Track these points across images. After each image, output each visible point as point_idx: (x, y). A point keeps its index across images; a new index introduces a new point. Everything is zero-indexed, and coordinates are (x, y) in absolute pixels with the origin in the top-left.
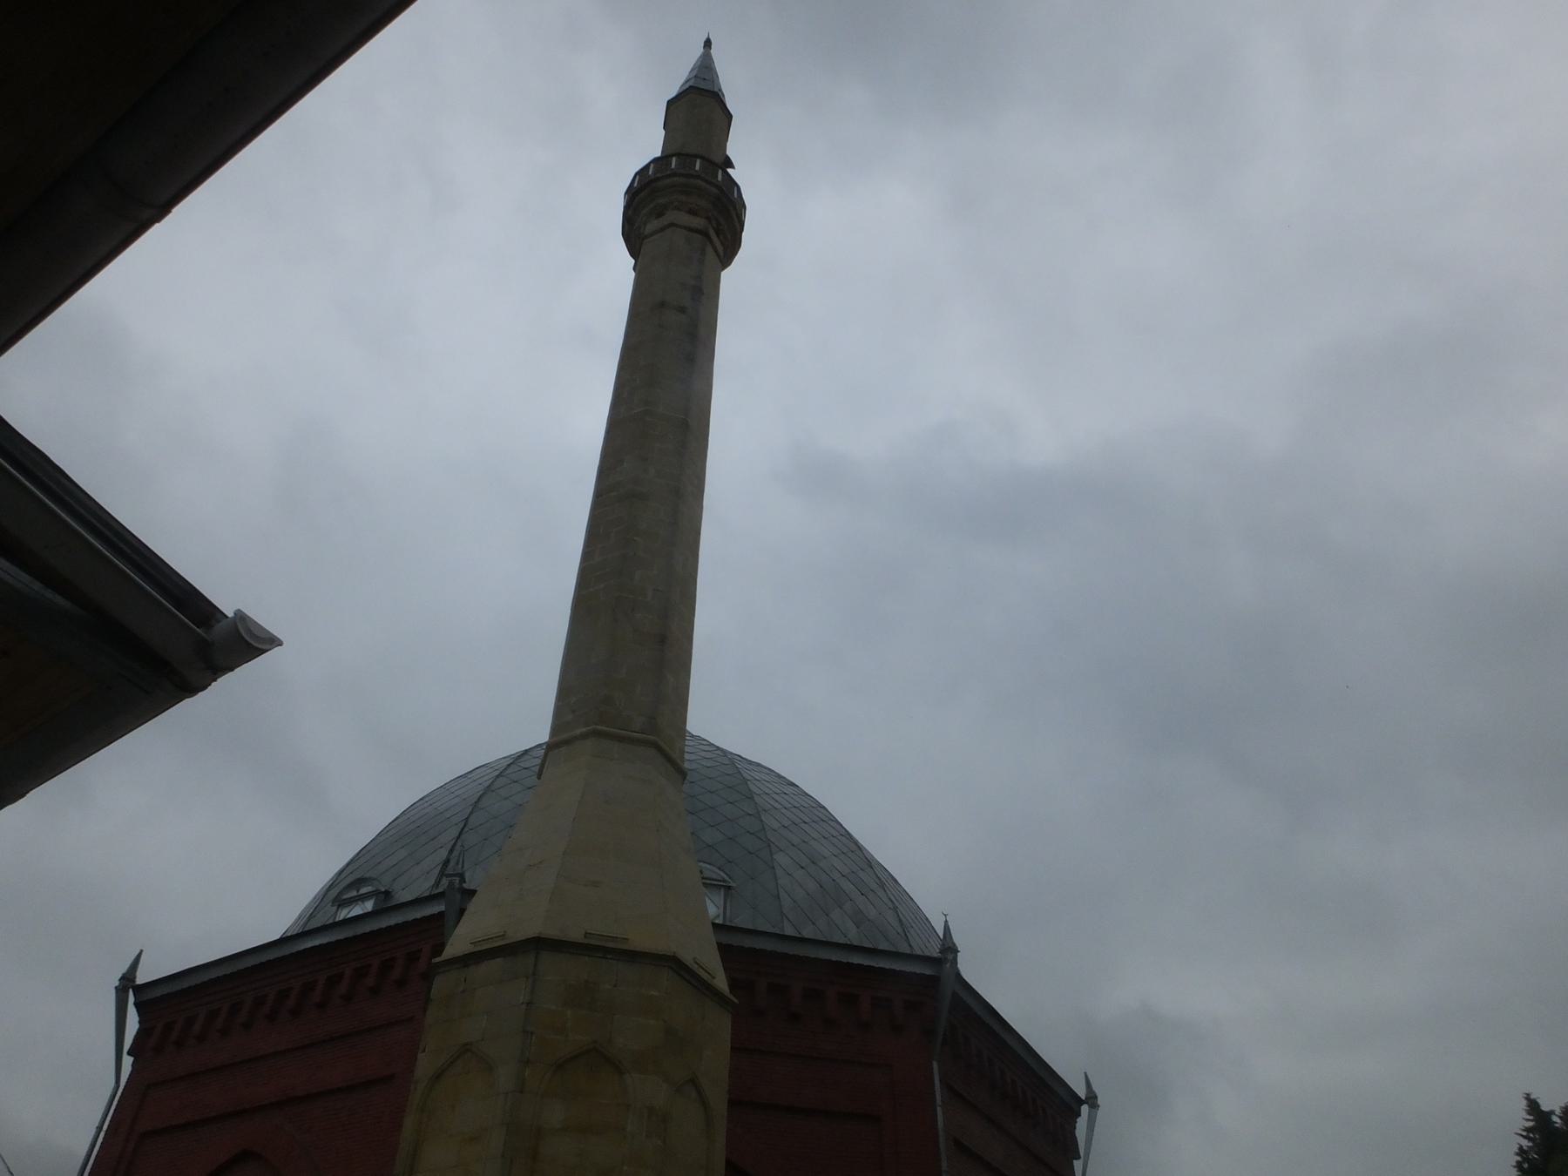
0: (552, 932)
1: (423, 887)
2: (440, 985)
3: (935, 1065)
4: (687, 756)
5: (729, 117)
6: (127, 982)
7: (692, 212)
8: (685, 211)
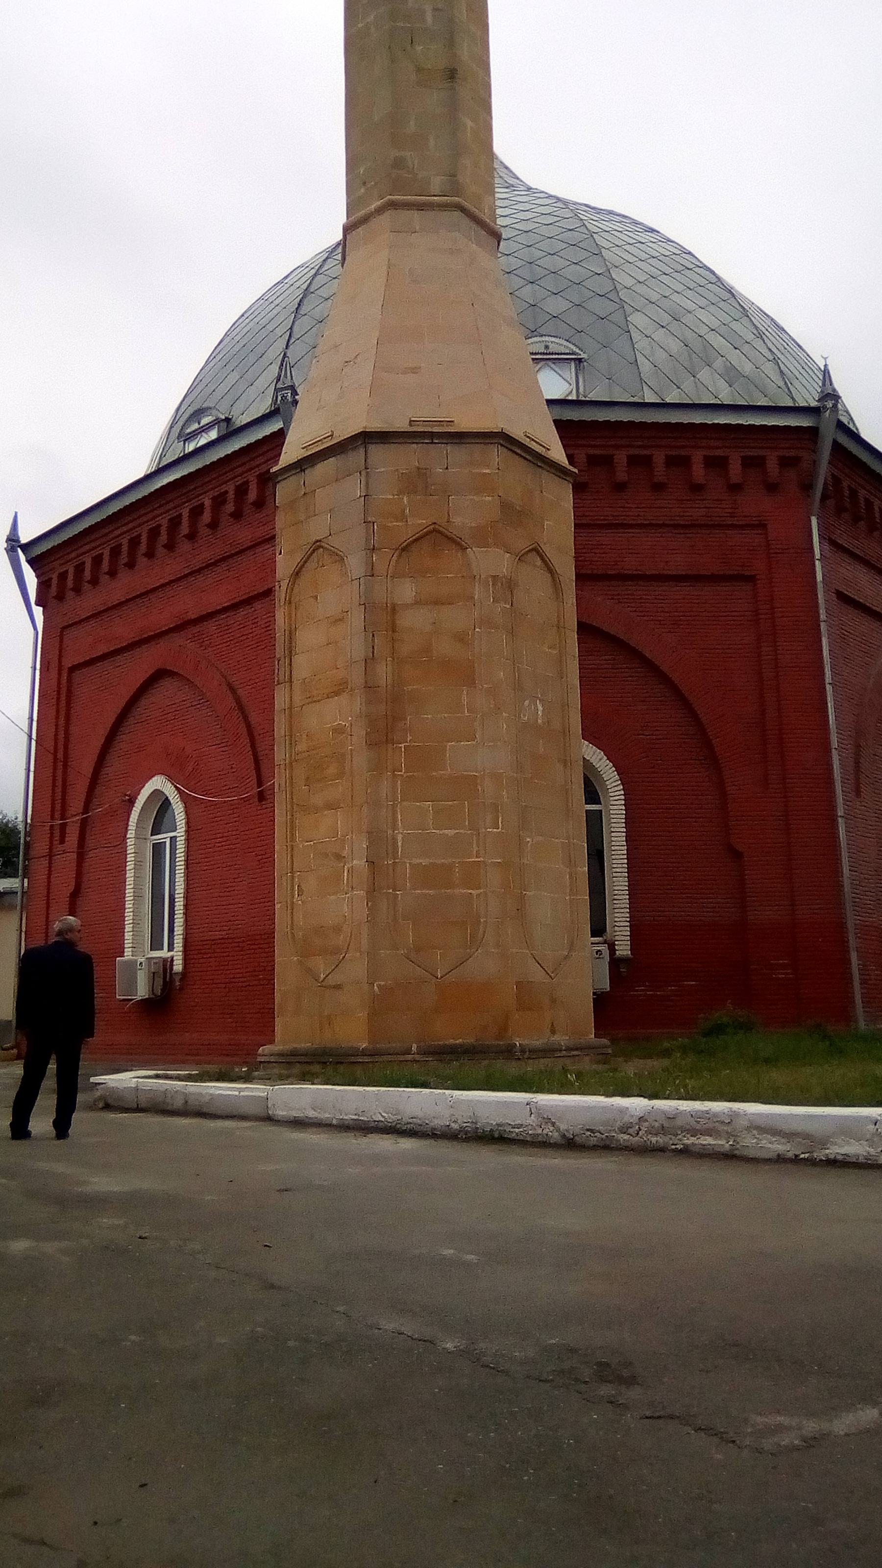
0: (376, 425)
1: (264, 406)
2: (283, 492)
3: (814, 521)
4: (499, 211)
6: (13, 543)
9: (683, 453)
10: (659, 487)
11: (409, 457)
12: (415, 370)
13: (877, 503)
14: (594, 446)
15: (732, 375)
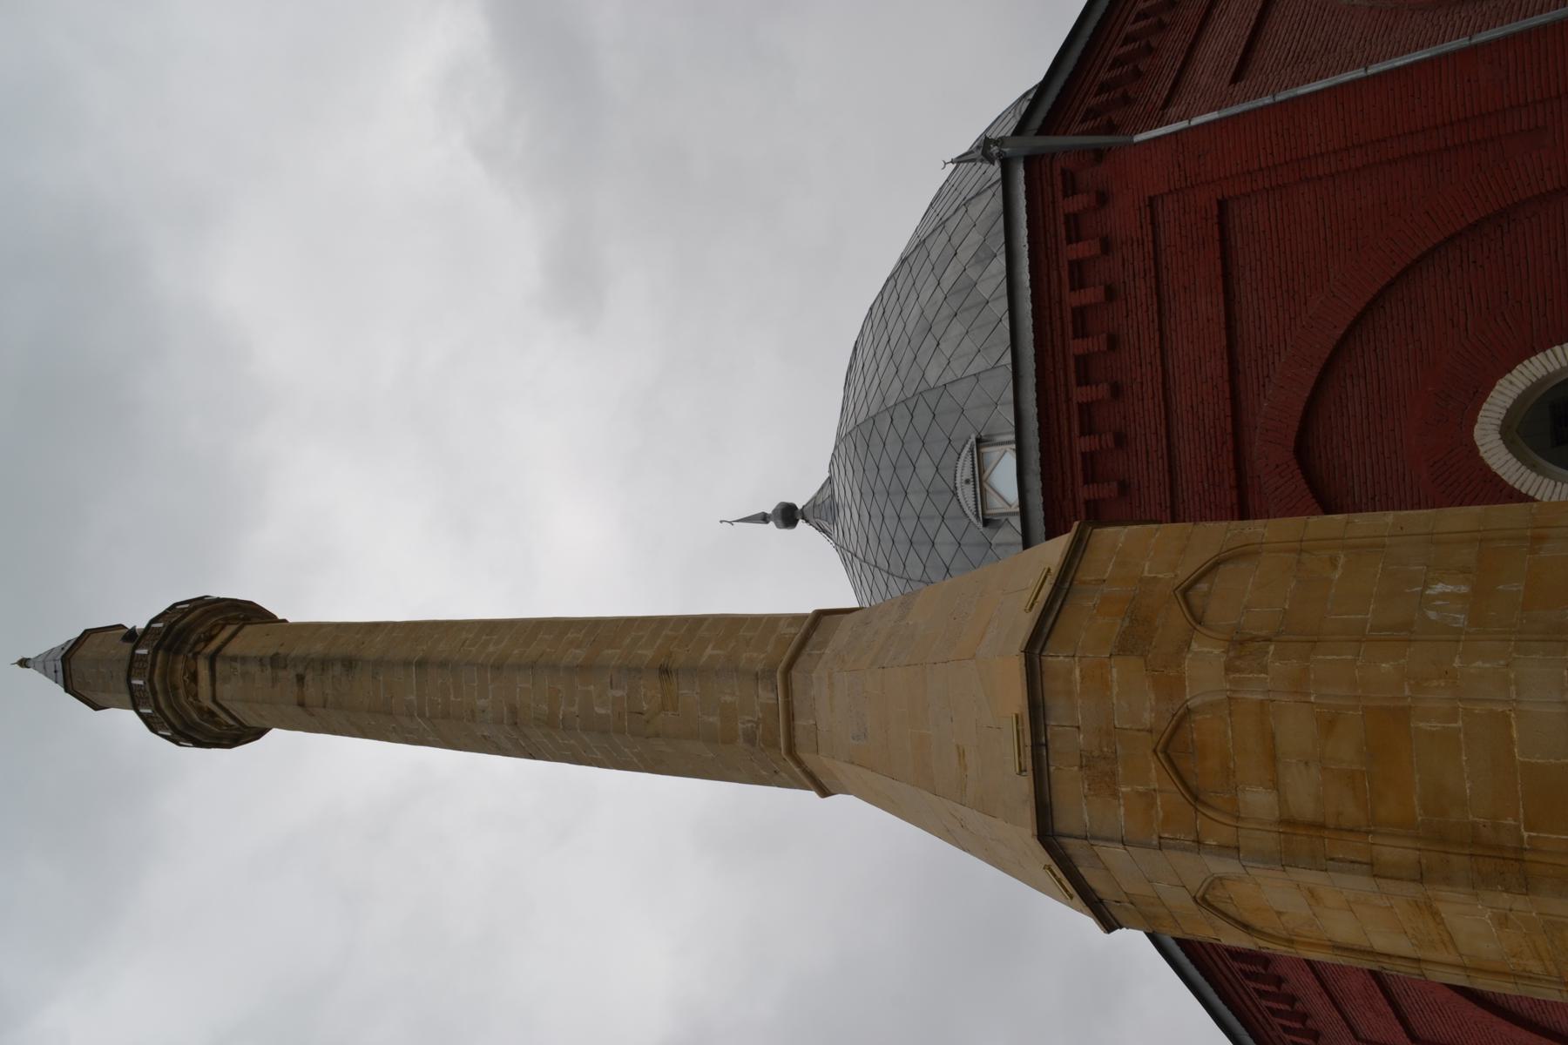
0: (1028, 814)
3: (1139, 138)
5: (88, 633)
7: (194, 677)
8: (201, 672)
9: (1068, 317)
10: (1113, 342)
11: (1068, 782)
12: (961, 754)
13: (1141, 6)
14: (1070, 430)
15: (982, 257)
